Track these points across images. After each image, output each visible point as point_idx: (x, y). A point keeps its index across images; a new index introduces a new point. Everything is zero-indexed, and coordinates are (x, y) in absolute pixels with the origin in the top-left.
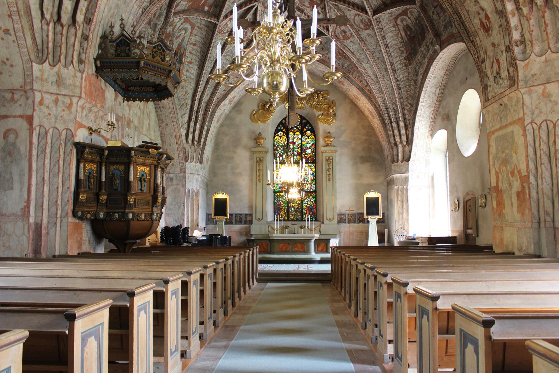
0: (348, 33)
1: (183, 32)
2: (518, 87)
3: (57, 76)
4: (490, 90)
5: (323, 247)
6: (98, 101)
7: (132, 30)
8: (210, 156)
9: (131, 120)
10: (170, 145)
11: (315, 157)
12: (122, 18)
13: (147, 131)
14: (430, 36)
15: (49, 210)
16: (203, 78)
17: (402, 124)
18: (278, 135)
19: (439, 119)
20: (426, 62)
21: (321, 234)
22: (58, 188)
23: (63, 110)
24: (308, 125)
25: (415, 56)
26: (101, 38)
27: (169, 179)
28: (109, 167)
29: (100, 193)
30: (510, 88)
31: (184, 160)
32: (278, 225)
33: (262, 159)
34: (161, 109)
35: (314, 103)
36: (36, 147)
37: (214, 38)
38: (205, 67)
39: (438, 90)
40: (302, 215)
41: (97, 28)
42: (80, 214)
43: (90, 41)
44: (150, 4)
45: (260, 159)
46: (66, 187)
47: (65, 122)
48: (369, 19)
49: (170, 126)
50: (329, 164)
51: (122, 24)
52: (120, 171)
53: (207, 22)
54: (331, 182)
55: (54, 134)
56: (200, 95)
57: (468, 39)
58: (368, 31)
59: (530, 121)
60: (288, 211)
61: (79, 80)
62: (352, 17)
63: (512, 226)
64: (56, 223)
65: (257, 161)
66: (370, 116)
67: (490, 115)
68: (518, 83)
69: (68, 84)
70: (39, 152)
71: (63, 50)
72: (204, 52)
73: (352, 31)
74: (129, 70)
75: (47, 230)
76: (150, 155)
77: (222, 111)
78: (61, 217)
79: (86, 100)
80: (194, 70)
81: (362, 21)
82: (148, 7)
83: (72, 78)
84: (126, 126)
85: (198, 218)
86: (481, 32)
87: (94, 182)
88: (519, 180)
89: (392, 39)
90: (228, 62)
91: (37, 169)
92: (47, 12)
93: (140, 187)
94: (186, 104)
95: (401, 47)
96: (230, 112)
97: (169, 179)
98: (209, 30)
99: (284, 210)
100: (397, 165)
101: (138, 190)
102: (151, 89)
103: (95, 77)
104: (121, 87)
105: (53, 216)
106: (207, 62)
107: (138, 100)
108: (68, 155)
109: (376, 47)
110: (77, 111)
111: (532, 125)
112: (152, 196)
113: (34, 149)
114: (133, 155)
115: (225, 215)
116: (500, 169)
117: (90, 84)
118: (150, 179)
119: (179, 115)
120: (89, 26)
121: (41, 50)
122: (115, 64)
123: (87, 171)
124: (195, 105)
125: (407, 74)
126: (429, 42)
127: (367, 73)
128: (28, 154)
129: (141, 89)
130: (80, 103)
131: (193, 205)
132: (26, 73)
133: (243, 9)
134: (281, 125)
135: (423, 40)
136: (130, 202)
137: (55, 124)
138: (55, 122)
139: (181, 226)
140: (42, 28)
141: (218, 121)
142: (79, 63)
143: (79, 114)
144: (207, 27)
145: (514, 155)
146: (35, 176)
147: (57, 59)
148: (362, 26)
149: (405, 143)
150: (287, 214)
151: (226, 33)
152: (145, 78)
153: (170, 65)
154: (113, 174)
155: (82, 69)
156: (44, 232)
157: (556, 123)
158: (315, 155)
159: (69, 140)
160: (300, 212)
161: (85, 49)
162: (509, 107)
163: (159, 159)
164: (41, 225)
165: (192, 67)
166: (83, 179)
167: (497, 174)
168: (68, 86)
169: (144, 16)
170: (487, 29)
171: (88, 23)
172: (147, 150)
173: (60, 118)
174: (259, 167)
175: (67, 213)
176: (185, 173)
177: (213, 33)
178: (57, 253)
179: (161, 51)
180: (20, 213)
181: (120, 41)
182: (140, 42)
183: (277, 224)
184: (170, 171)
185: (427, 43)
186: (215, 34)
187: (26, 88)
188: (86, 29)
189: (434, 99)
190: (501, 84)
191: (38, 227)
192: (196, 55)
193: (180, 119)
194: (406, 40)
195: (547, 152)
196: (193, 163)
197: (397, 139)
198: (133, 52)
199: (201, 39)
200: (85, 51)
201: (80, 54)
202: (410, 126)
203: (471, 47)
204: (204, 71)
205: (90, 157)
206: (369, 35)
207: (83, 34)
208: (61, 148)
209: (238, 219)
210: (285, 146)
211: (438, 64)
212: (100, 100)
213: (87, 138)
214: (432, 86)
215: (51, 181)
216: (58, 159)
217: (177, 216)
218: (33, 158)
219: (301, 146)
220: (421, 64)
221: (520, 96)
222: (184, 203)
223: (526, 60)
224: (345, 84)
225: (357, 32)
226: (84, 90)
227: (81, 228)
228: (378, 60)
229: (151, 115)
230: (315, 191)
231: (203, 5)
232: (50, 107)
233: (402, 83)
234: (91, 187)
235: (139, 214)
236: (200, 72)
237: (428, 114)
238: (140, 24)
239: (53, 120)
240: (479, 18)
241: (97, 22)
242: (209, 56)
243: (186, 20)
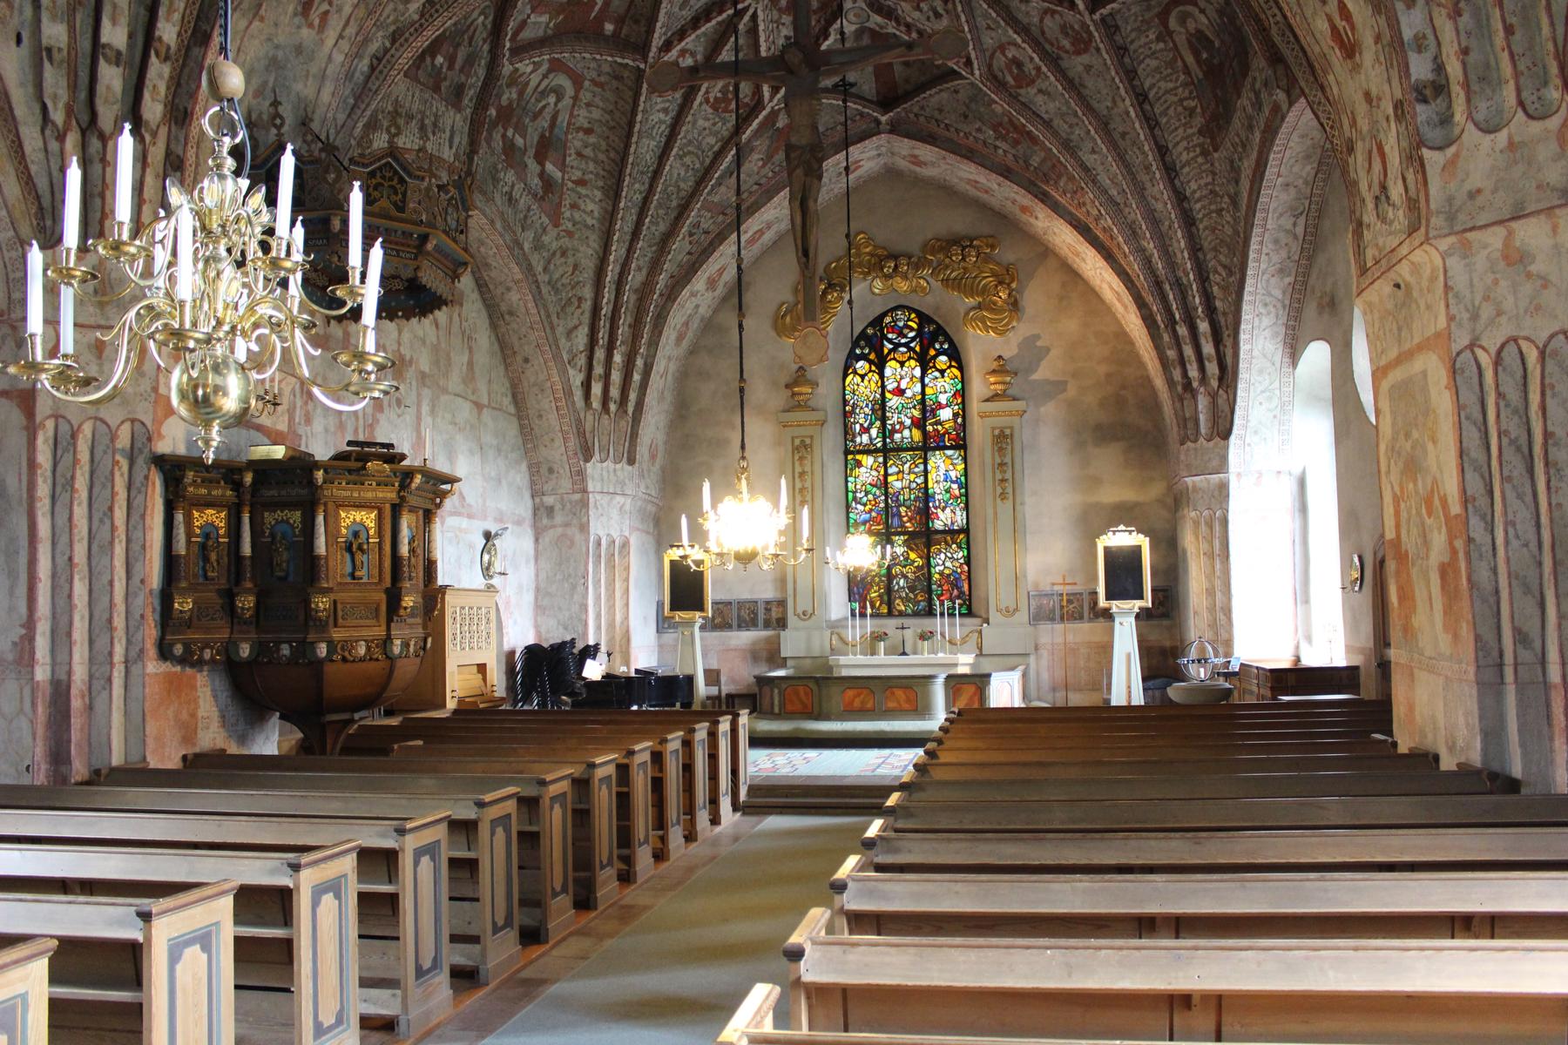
0: (1028, 68)
1: (552, 99)
2: (1427, 233)
4: (1370, 238)
5: (971, 699)
8: (660, 438)
9: (408, 358)
11: (964, 431)
13: (464, 382)
14: (1259, 63)
15: (91, 642)
17: (1203, 326)
18: (855, 372)
19: (1310, 311)
20: (1258, 140)
21: (980, 654)
22: (111, 583)
24: (941, 338)
25: (1229, 122)
27: (542, 509)
29: (235, 590)
30: (1409, 235)
31: (581, 457)
32: (858, 630)
33: (808, 441)
34: (507, 317)
35: (954, 275)
36: (49, 473)
37: (641, 108)
39: (1302, 221)
40: (930, 601)
42: (178, 650)
44: (393, 43)
45: (802, 441)
46: (136, 580)
48: (1084, 25)
50: (1000, 449)
54: (1009, 503)
57: (1312, 79)
58: (1085, 59)
59: (1466, 342)
60: (889, 590)
62: (1036, 20)
63: (1431, 670)
64: (110, 680)
65: (796, 449)
66: (1118, 305)
67: (1376, 316)
68: (1428, 221)
70: (58, 489)
73: (1037, 59)
75: (87, 700)
78: (126, 662)
81: (1064, 29)
82: (386, 51)
85: (627, 618)
86: (1336, 57)
87: (218, 561)
88: (1444, 530)
89: (1158, 76)
90: (690, 173)
91: (54, 535)
92: (55, 104)
93: (349, 569)
94: (580, 299)
95: (1186, 99)
96: (716, 311)
97: (542, 509)
99: (878, 585)
100: (1196, 449)
105: (99, 660)
106: (627, 178)
109: (1114, 101)
111: (1473, 353)
113: (40, 481)
116: (1402, 489)
119: (560, 330)
121: (50, 210)
125: (1209, 179)
126: (1259, 79)
127: (1093, 181)
128: (25, 496)
132: (11, 276)
133: (714, 22)
134: (862, 343)
135: (1245, 75)
139: (573, 641)
140: (46, 150)
141: (680, 338)
145: (1430, 446)
146: (49, 555)
148: (1066, 43)
149: (1215, 383)
150: (886, 598)
156: (76, 703)
157: (1545, 346)
158: (964, 425)
159: (141, 451)
160: (922, 591)
162: (1415, 294)
164: (69, 687)
165: (587, 196)
166: (185, 557)
167: (1397, 501)
169: (377, 79)
170: (1350, 50)
172: (360, 464)
174: (801, 465)
176: (585, 491)
178: (117, 759)
180: (10, 657)
183: (854, 627)
184: (545, 488)
185: (1253, 85)
187: (13, 316)
189: (1294, 250)
190: (1392, 222)
191: (60, 692)
192: (596, 161)
193: (563, 342)
194: (1201, 76)
195: (1523, 441)
196: (609, 464)
197: (1193, 373)
202: (1225, 334)
203: (1320, 103)
204: (622, 205)
205: (204, 491)
206: (1088, 68)
208: (117, 474)
209: (745, 614)
210: (875, 401)
211: (1291, 144)
214: (1280, 210)
215: (93, 564)
217: (567, 614)
218: (39, 505)
219: (923, 402)
220: (1244, 146)
221: (1438, 261)
222: (585, 577)
223: (1449, 145)
224: (1039, 216)
225: (1054, 62)
227: (194, 687)
228: (1124, 139)
229: (476, 336)
230: (965, 531)
231: (600, 20)
233: (1198, 206)
234: (209, 574)
235: (348, 644)
236: (610, 208)
237: (1278, 293)
238: (367, 101)
240: (1327, 15)
242: (630, 160)
243: (556, 66)
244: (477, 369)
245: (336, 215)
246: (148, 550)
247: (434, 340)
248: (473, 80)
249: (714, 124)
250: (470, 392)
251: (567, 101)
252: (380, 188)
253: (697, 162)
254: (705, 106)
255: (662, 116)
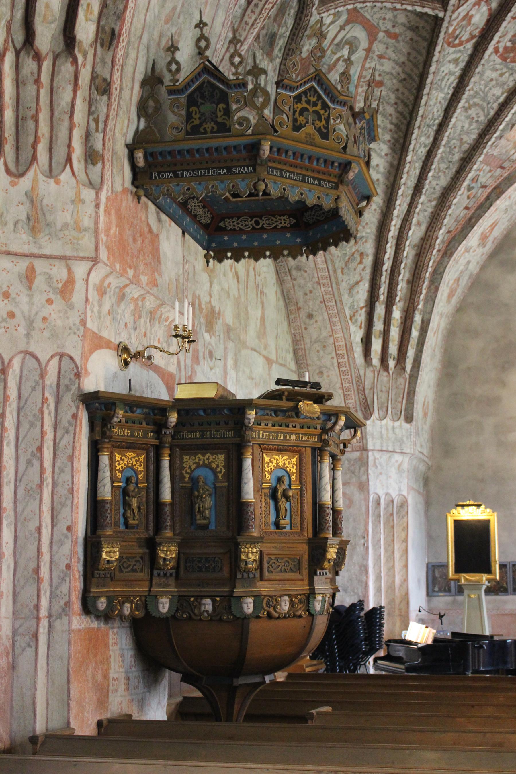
1: (345, 52)
3: (28, 205)
6: (142, 267)
7: (169, 59)
9: (217, 310)
10: (321, 373)
12: (201, 21)
13: (258, 338)
15: (15, 594)
16: (405, 176)
22: (39, 530)
23: (50, 302)
26: (144, 83)
28: (182, 462)
29: (158, 540)
34: (294, 272)
37: (435, 59)
38: (411, 147)
41: (133, 55)
42: (102, 604)
43: (115, 94)
46: (62, 527)
47: (54, 336)
49: (320, 318)
51: (202, 37)
52: (214, 472)
53: (412, 17)
55: (25, 372)
56: (398, 226)
61: (90, 209)
64: (36, 636)
69: (59, 226)
71: (44, 128)
72: (405, 105)
74: (229, 170)
76: (300, 420)
77: (462, 268)
78: (50, 616)
79: (112, 266)
80: (381, 157)
83: (70, 207)
84: (203, 329)
85: (406, 580)
87: (139, 508)
90: (474, 125)
96: (483, 268)
98: (418, 39)
101: (267, 525)
102: (285, 221)
103: (130, 197)
104: (199, 223)
106: (416, 131)
107: (249, 257)
108: (67, 432)
110: (87, 300)
112: (310, 542)
114: (252, 421)
115: (487, 569)
117: (120, 218)
118: (301, 490)
119: (344, 286)
120: (111, 53)
122: (188, 157)
123: (119, 475)
124: (387, 256)
129: (257, 223)
130: (95, 278)
131: (390, 543)
136: (246, 563)
137: (28, 343)
138: (28, 336)
139: (361, 603)
141: (451, 295)
142: (86, 161)
143: (92, 311)
144: (414, 29)
147: (26, 154)
151: (468, 41)
152: (275, 192)
153: (345, 148)
154: (194, 481)
155: (95, 177)
161: (102, 119)
163: (325, 431)
166: (111, 501)
168: (61, 230)
169: (253, 12)
171: (106, 44)
172: (291, 404)
173: (42, 326)
175: (67, 604)
177: (432, 44)
179: (318, 108)
181: (199, 88)
182: (257, 87)
186: (438, 49)
188: (103, 62)
193: (345, 297)
196: (388, 422)
198: (239, 114)
199: (397, 67)
200: (101, 126)
201: (88, 136)
204: (409, 159)
205: (127, 432)
207: (93, 78)
212: (146, 264)
213: (115, 375)
215: (20, 508)
216: (38, 443)
222: (365, 537)
226: (105, 239)
227: (107, 645)
232: (13, 295)
234: (131, 522)
236: (396, 163)
239: (22, 330)
241: (133, 39)
242: (420, 113)
244: (267, 324)
245: (265, 139)
246: (75, 494)
247: (236, 293)
248: (282, 30)
249: (501, 75)
250: (262, 347)
251: (360, 54)
252: (305, 113)
253: (481, 113)
254: (495, 57)
255: (452, 66)
